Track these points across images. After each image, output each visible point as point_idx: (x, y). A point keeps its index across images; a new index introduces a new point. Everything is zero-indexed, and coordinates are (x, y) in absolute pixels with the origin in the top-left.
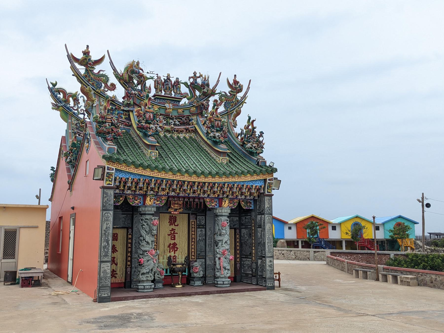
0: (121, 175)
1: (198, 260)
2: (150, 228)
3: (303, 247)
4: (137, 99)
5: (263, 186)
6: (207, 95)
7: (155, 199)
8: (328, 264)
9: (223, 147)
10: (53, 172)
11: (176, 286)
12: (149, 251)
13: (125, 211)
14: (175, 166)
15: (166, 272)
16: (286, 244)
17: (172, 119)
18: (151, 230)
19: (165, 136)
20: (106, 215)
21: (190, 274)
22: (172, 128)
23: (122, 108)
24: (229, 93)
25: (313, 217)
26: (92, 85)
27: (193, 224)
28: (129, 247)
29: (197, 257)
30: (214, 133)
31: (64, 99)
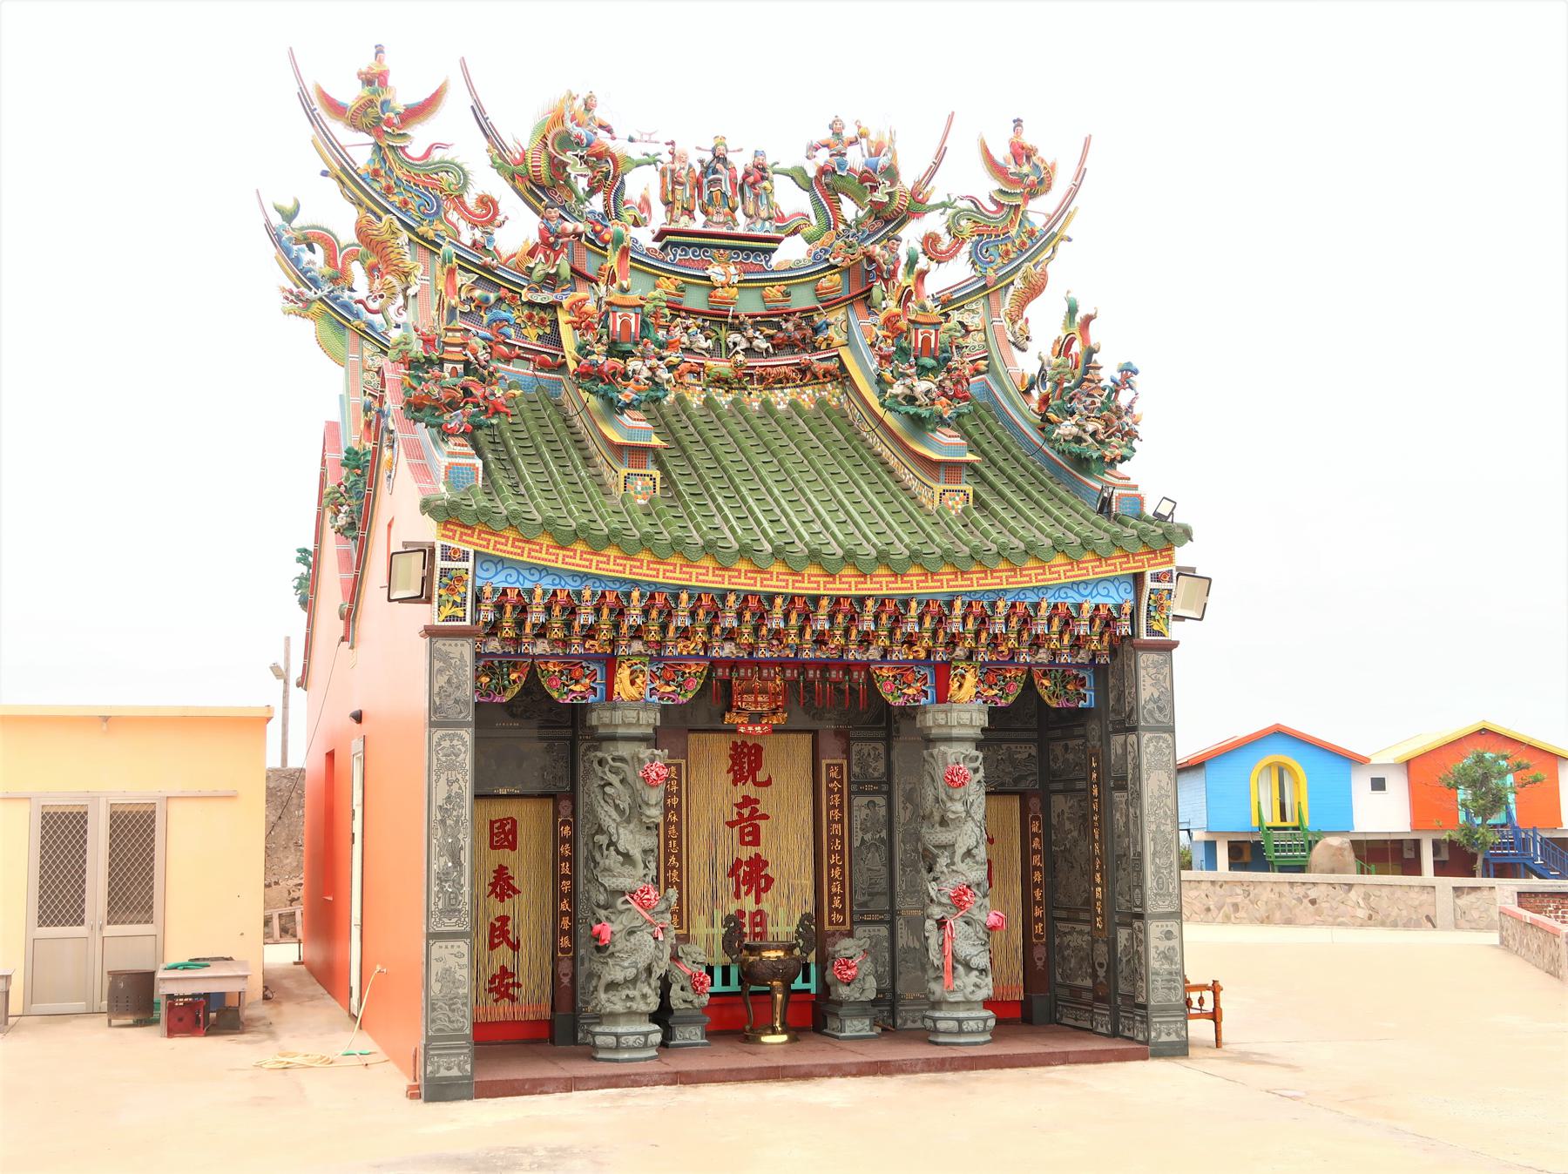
0: (501, 577)
1: (860, 931)
2: (634, 794)
3: (1441, 869)
4: (585, 254)
5: (1127, 610)
6: (889, 218)
7: (653, 676)
8: (1503, 941)
9: (945, 444)
10: (304, 569)
11: (765, 1039)
12: (632, 893)
13: (530, 723)
14: (728, 534)
15: (726, 981)
16: (1350, 857)
17: (738, 328)
18: (638, 806)
19: (709, 403)
20: (446, 744)
21: (825, 988)
22: (737, 366)
23: (526, 295)
24: (992, 199)
25: (1484, 732)
26: (399, 209)
27: (833, 775)
28: (565, 877)
29: (856, 918)
30: (908, 381)
31: (328, 271)
